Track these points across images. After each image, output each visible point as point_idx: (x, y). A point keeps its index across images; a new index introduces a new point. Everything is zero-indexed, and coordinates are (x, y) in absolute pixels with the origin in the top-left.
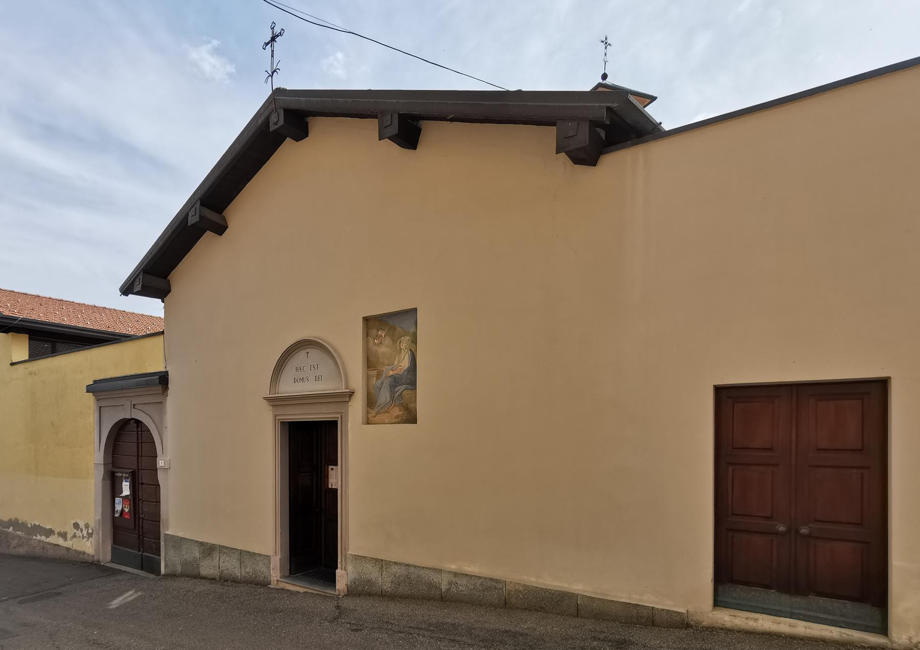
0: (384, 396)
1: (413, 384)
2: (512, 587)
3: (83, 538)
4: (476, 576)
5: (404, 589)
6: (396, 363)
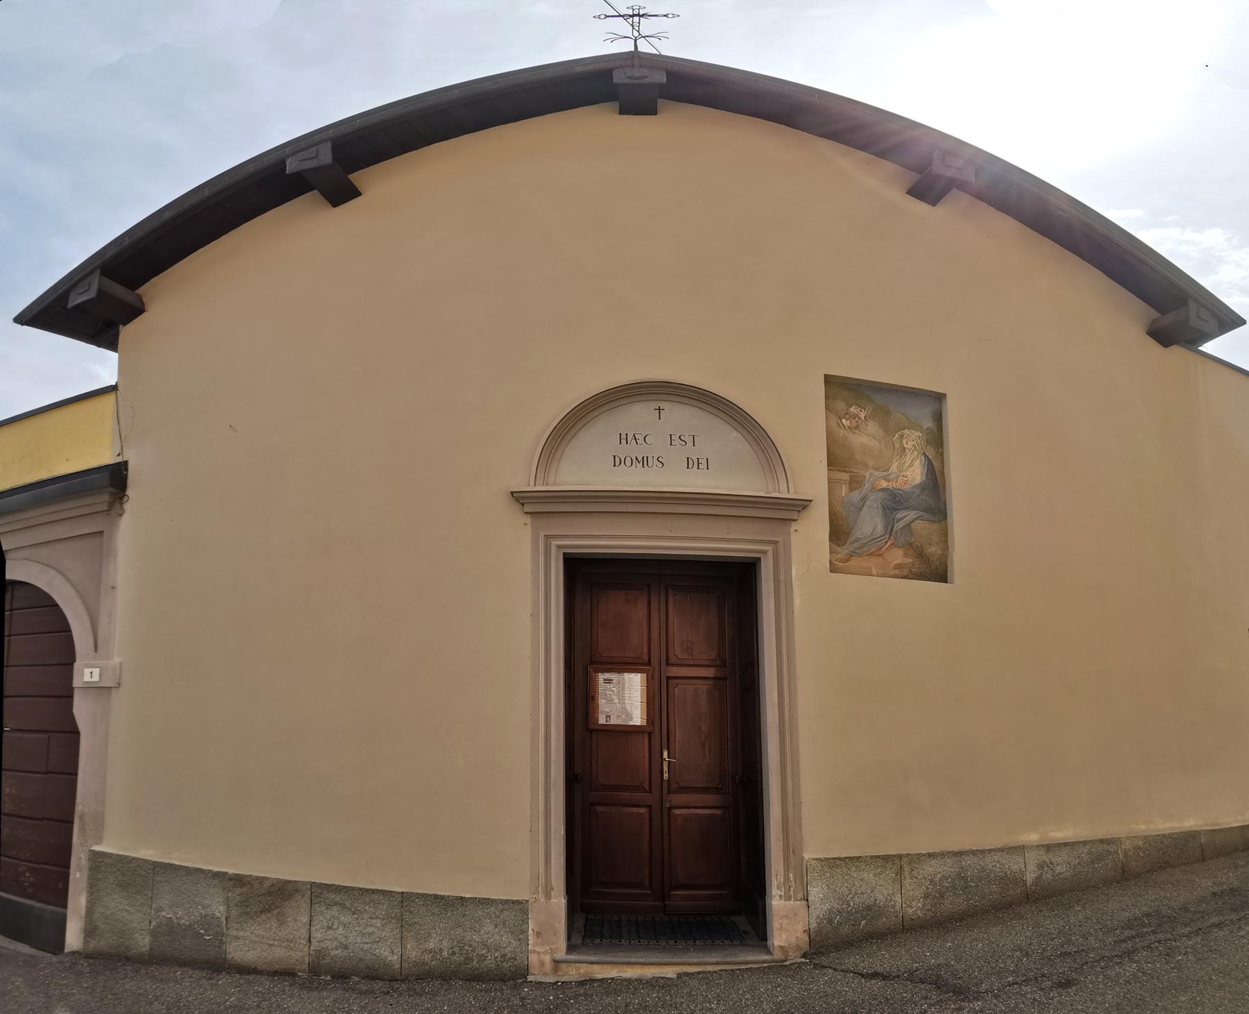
0: (870, 523)
1: (938, 511)
2: (1129, 844)
4: (1080, 842)
5: (951, 904)
6: (894, 468)
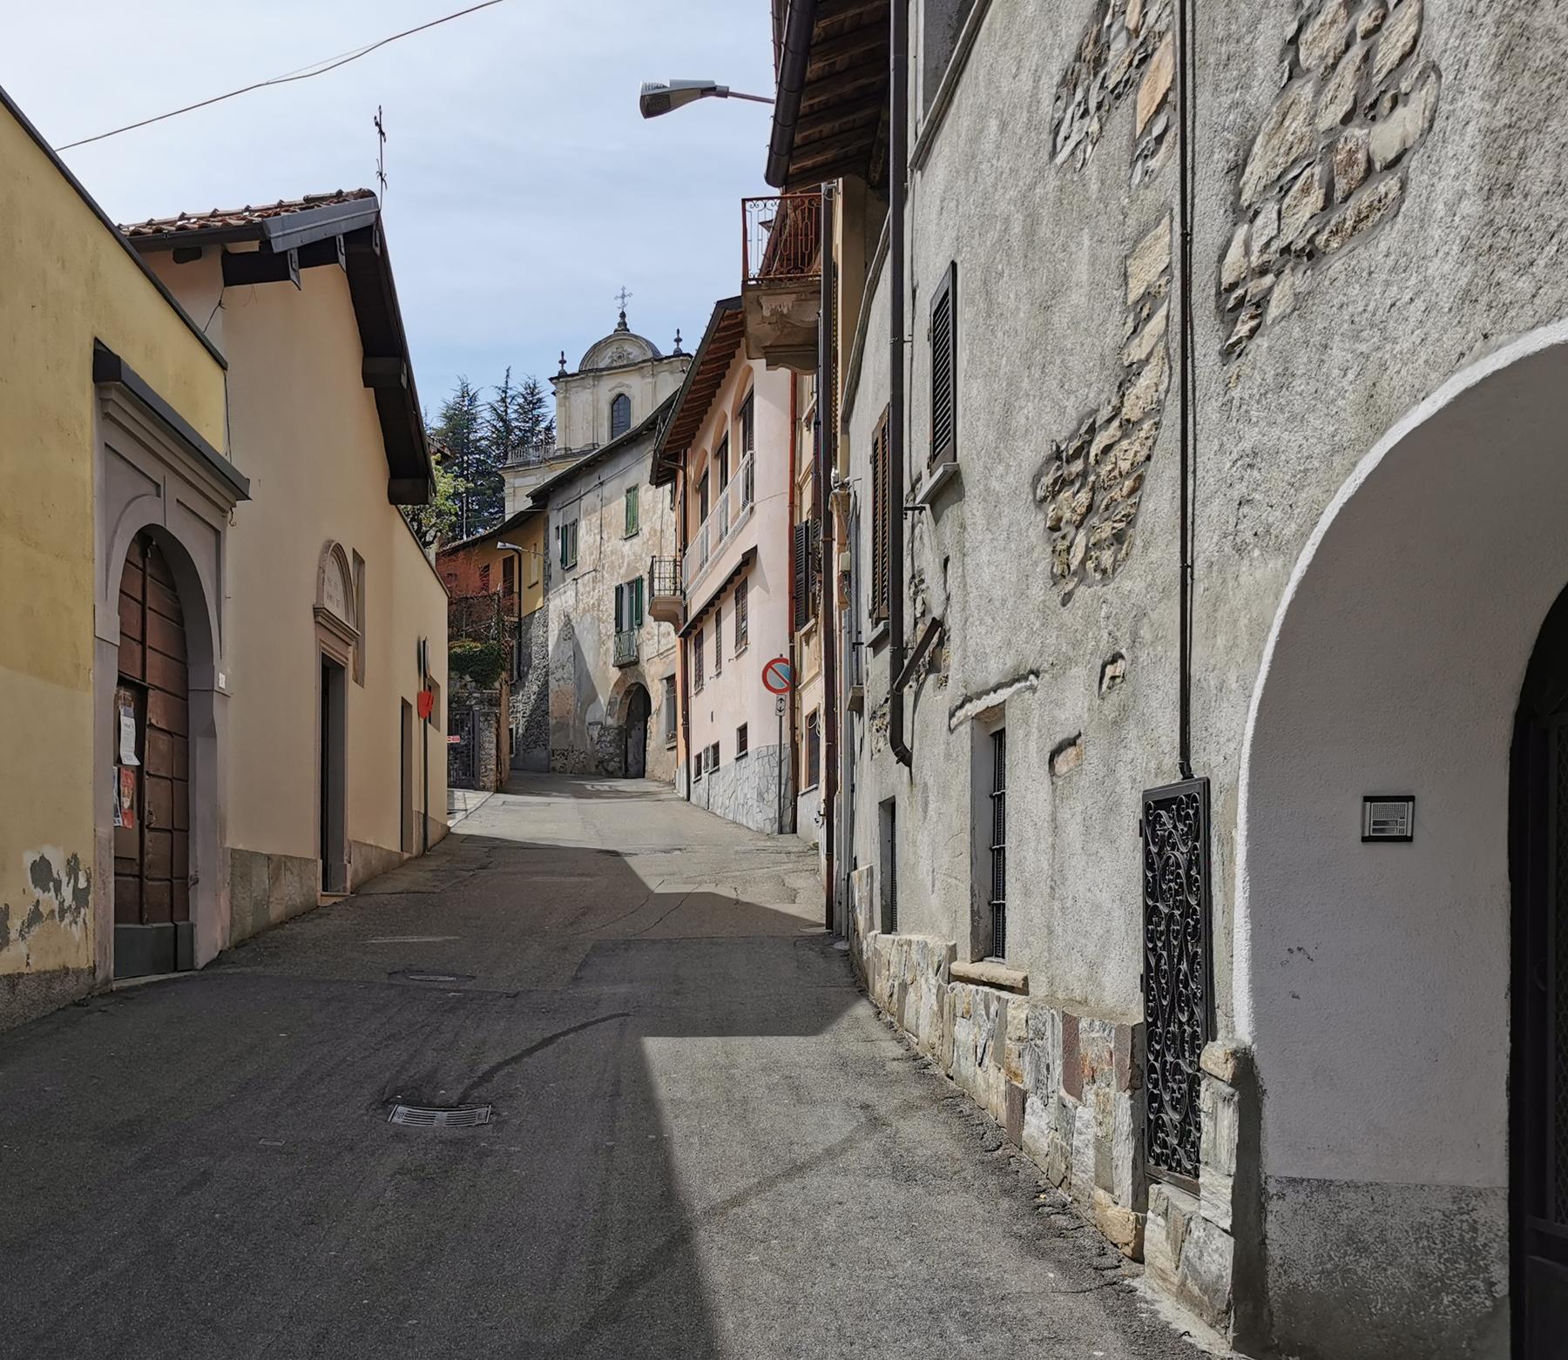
3: (63, 912)
